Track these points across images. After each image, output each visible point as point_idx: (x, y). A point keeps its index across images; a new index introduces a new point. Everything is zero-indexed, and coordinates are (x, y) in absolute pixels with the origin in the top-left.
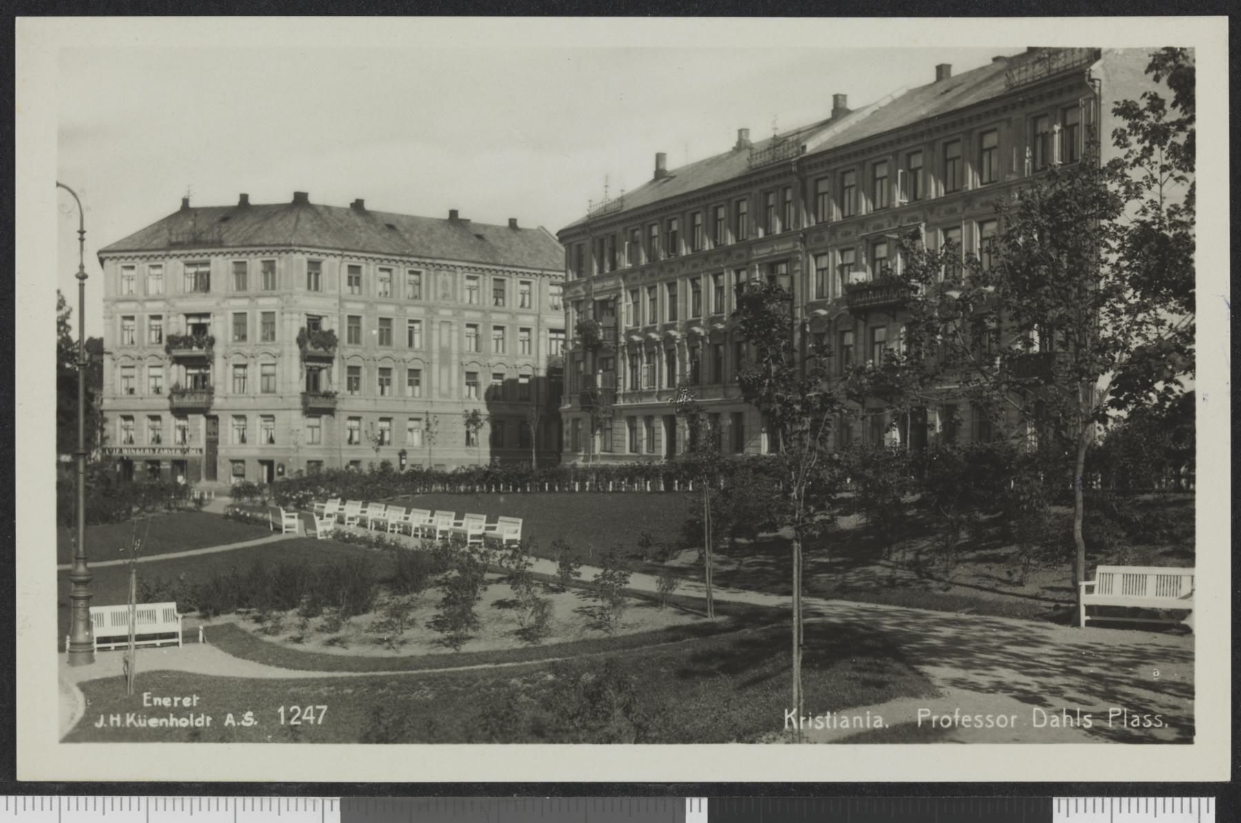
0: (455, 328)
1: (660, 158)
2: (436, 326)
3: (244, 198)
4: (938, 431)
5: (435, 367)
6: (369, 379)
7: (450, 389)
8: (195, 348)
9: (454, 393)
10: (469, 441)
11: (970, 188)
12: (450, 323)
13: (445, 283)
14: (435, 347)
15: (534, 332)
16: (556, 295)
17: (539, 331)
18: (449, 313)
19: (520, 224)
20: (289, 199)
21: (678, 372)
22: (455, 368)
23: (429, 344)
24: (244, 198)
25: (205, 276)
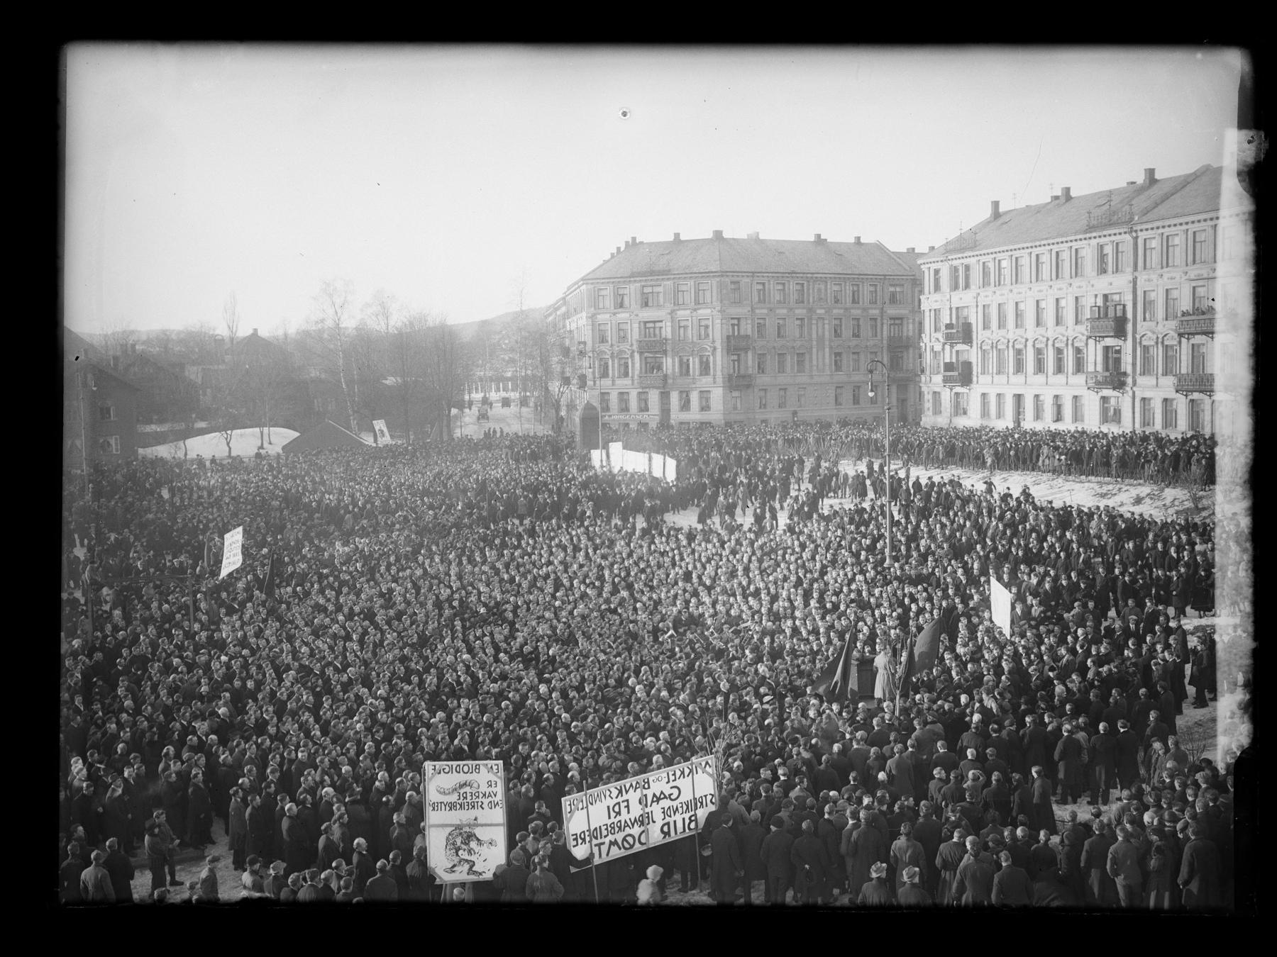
0: (826, 322)
1: (996, 204)
2: (814, 322)
3: (677, 235)
4: (904, 872)
5: (814, 350)
6: (771, 363)
7: (824, 365)
8: (507, 358)
9: (827, 368)
10: (837, 402)
11: (1152, 903)
12: (823, 319)
13: (819, 290)
14: (814, 336)
15: (879, 321)
16: (707, 274)
17: (882, 319)
18: (823, 311)
19: (862, 241)
20: (710, 236)
21: (815, 363)
22: (827, 350)
23: (810, 335)
24: (677, 235)
25: (1147, 316)
